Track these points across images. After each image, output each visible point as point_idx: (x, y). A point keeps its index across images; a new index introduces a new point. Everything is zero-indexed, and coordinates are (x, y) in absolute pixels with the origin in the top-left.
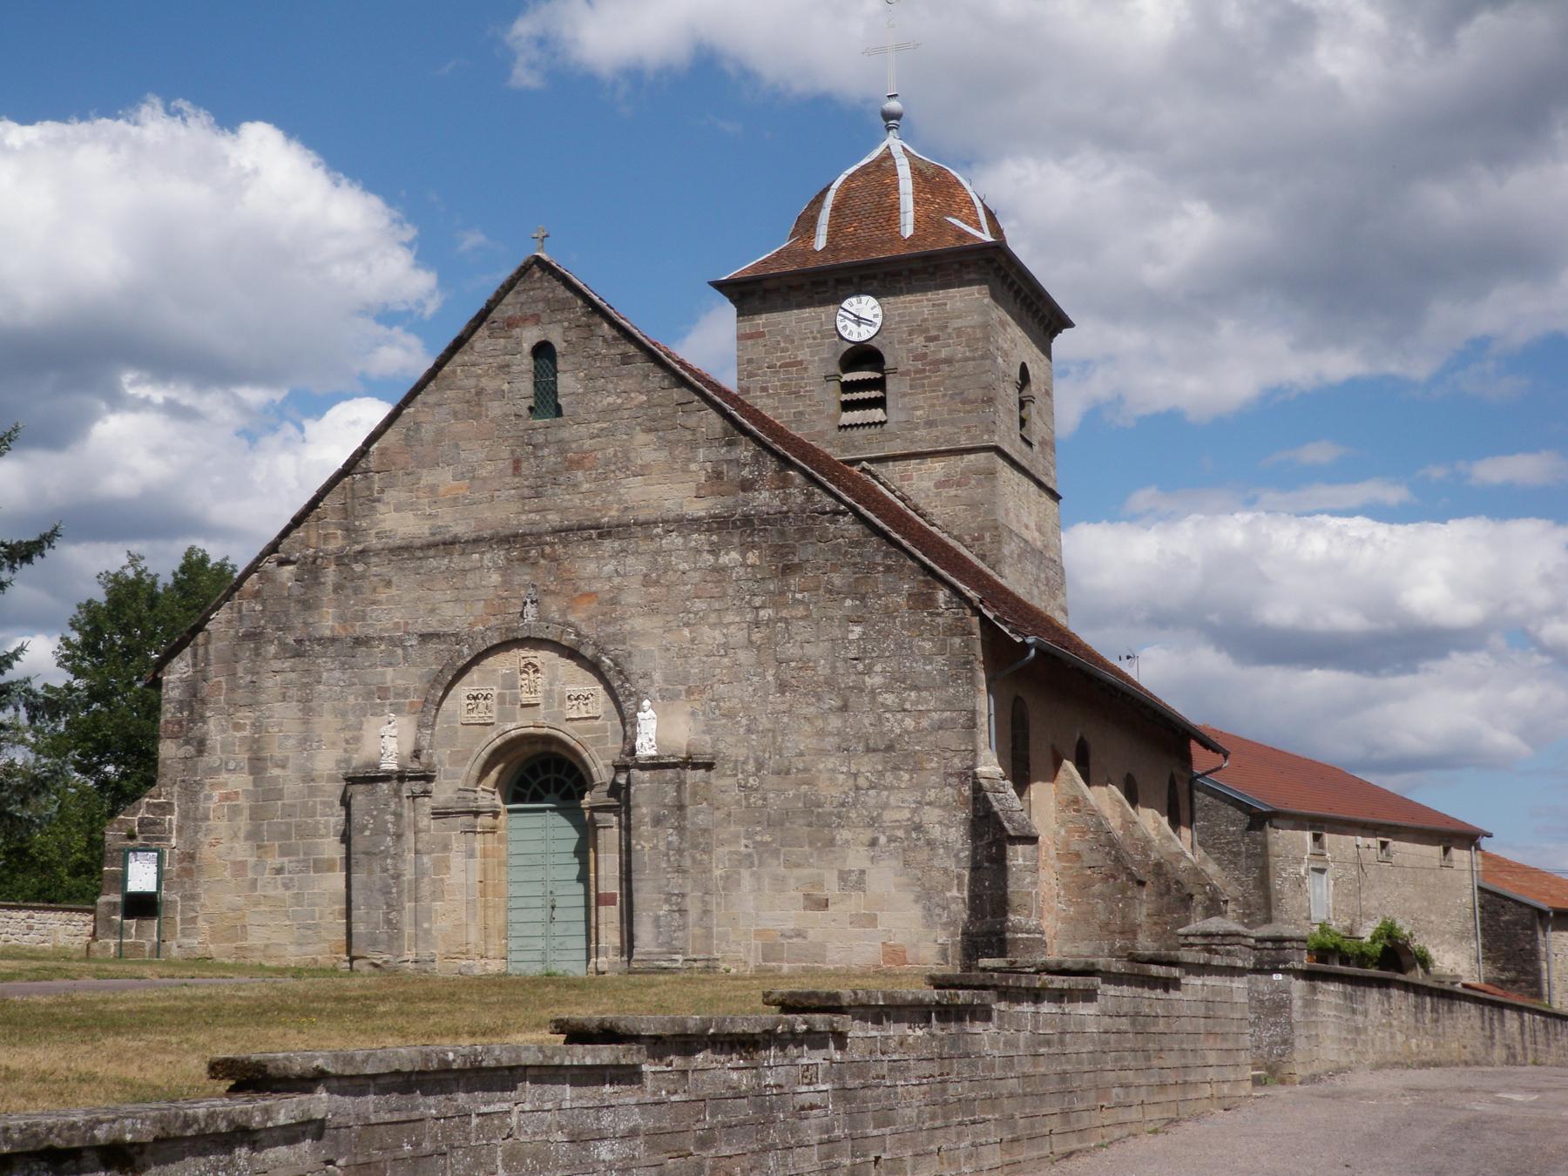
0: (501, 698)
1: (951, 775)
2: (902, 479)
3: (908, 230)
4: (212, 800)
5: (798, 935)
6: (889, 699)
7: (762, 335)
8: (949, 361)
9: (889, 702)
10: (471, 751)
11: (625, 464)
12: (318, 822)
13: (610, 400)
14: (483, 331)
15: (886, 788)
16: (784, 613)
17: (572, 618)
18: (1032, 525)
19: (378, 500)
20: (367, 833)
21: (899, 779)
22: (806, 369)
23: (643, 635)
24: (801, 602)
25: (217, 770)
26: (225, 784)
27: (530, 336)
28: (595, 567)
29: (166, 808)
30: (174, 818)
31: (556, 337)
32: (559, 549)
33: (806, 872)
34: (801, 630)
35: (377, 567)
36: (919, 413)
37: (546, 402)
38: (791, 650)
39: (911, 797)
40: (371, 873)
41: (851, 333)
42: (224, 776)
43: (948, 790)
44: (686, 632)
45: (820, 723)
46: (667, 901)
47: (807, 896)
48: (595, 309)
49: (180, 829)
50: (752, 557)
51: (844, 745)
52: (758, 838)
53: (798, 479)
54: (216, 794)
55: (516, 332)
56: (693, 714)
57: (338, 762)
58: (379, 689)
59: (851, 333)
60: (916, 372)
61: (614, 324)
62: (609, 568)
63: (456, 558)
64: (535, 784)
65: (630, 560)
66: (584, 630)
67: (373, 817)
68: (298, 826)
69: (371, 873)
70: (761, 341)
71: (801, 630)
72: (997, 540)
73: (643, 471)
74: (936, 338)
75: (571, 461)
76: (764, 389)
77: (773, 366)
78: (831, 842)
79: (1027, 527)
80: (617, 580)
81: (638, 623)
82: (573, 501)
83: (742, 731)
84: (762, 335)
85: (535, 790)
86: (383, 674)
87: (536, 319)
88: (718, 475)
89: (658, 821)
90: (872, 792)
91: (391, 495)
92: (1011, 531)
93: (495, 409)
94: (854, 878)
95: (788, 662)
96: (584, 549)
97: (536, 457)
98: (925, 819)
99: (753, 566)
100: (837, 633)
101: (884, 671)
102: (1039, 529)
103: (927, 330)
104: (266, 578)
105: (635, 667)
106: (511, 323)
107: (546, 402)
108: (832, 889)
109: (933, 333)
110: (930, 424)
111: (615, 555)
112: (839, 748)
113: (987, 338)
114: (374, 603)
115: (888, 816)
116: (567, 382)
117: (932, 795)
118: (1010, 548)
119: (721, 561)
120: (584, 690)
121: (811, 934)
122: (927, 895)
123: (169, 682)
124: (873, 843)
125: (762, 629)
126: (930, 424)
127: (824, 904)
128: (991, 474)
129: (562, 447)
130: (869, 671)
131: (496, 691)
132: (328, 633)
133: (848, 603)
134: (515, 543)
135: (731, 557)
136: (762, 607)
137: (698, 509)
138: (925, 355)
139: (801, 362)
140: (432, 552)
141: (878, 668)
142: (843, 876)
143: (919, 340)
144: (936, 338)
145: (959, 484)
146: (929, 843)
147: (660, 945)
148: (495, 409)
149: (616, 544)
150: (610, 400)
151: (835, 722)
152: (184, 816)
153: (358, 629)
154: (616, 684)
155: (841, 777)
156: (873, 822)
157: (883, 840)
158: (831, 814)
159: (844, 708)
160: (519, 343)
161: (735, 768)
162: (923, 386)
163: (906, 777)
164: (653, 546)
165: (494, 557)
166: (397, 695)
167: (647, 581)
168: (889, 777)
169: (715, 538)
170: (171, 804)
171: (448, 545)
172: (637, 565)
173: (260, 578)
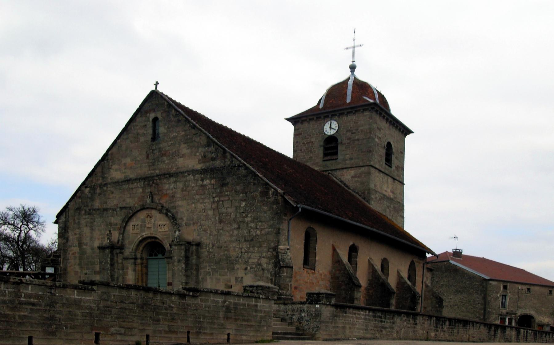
6: (253, 225)
7: (301, 134)
8: (358, 140)
11: (177, 154)
16: (222, 199)
27: (152, 116)
28: (168, 186)
31: (159, 116)
32: (158, 181)
34: (227, 204)
43: (269, 253)
45: (231, 233)
47: (226, 284)
62: (172, 186)
71: (227, 204)
78: (233, 269)
80: (174, 190)
81: (180, 203)
84: (301, 134)
87: (154, 111)
90: (246, 254)
94: (239, 279)
96: (165, 181)
98: (262, 262)
101: (251, 216)
106: (147, 112)
109: (354, 131)
116: (162, 130)
117: (264, 254)
120: (164, 223)
124: (246, 269)
130: (247, 216)
133: (241, 195)
134: (147, 180)
137: (199, 167)
141: (249, 215)
142: (236, 279)
144: (355, 133)
145: (359, 177)
151: (236, 232)
153: (105, 206)
157: (249, 268)
159: (239, 228)
160: (149, 118)
163: (257, 249)
164: (185, 179)
166: (114, 225)
172: (180, 185)
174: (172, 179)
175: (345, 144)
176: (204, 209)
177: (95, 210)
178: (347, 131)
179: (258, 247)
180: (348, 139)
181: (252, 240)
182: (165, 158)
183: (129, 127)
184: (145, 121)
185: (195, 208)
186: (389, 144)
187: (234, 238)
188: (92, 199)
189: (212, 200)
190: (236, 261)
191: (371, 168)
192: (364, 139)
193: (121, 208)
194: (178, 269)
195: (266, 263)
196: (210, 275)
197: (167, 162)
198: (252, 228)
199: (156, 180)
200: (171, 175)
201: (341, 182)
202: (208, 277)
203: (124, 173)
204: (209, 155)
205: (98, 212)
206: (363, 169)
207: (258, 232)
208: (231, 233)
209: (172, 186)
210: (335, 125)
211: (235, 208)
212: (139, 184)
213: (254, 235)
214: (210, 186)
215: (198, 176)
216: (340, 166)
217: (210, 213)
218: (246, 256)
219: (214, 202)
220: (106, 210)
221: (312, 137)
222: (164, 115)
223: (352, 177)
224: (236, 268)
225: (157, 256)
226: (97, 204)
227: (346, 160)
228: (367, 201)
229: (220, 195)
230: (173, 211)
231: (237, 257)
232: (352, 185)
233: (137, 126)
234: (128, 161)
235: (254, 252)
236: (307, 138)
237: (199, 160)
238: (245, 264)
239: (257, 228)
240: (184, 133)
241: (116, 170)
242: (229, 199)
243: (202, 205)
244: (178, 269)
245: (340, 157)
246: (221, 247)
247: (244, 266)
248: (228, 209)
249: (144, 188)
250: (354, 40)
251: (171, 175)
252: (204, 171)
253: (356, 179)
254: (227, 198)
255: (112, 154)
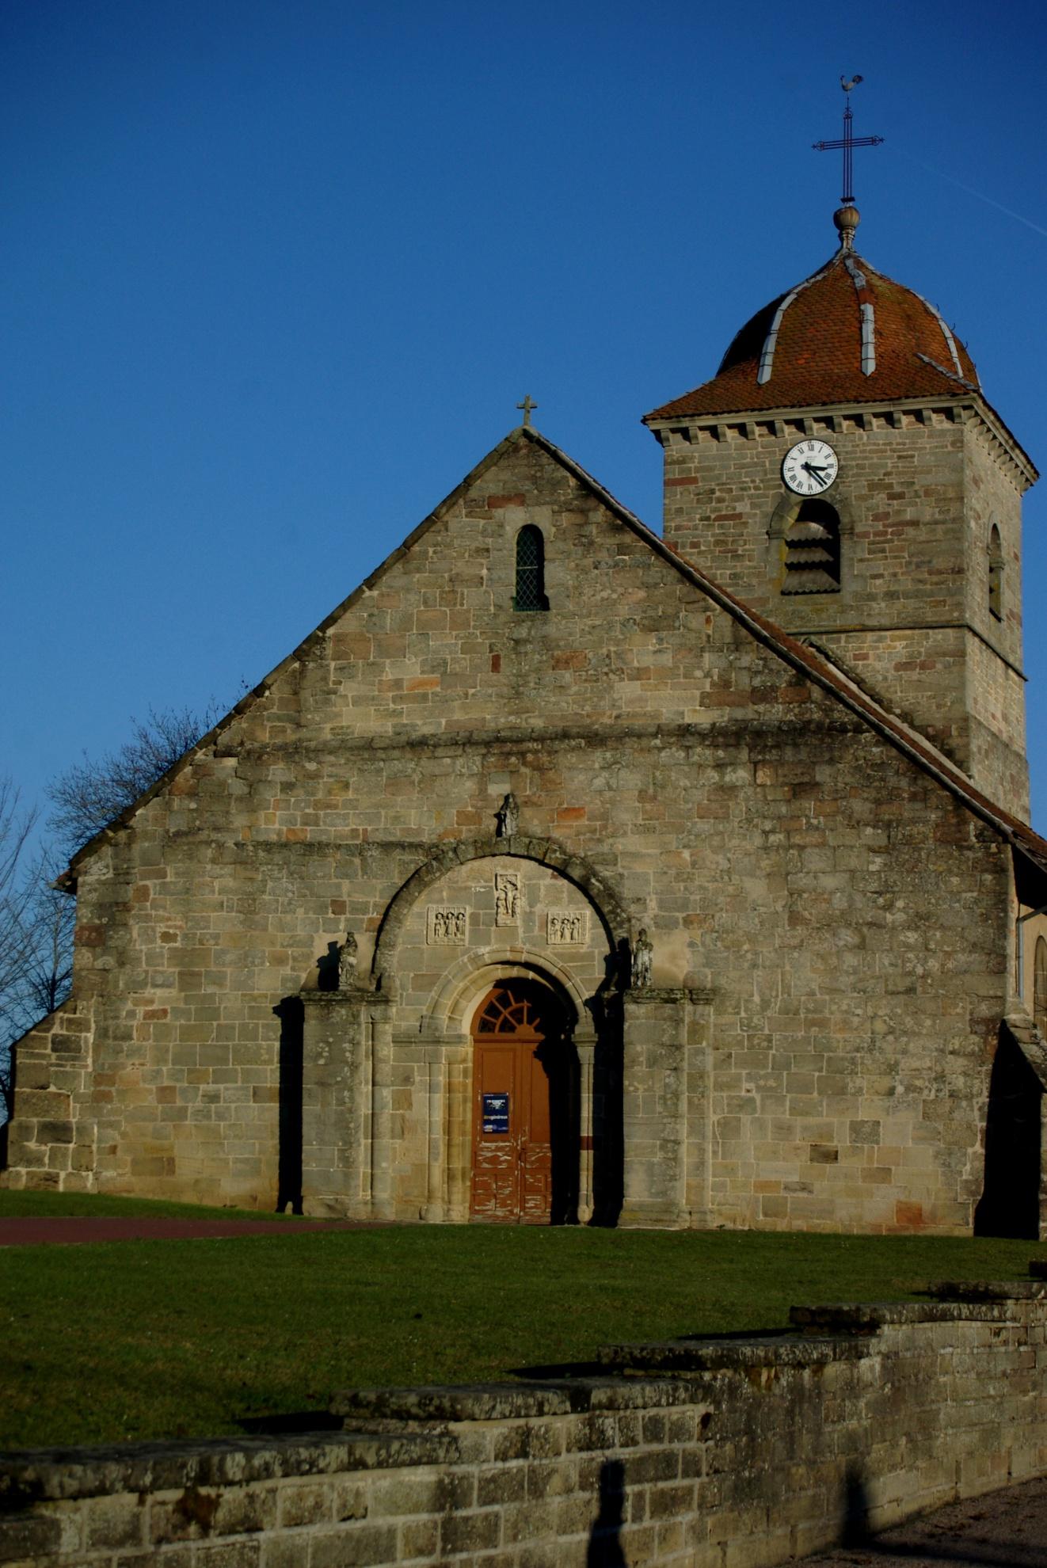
0: (474, 918)
1: (978, 1023)
2: (856, 658)
3: (870, 367)
4: (132, 1012)
5: (803, 1189)
6: (912, 937)
7: (694, 481)
8: (915, 523)
9: (911, 941)
10: (438, 976)
11: (615, 667)
12: (259, 1047)
13: (605, 594)
14: (461, 508)
15: (905, 1033)
16: (797, 839)
17: (556, 834)
18: (999, 715)
19: (335, 693)
20: (322, 1062)
21: (920, 1024)
22: (745, 523)
23: (635, 856)
24: (817, 828)
25: (143, 985)
26: (152, 1002)
27: (515, 518)
28: (583, 777)
29: (81, 1025)
30: (91, 1036)
31: (543, 518)
32: (544, 758)
33: (812, 1120)
34: (815, 860)
35: (333, 766)
36: (879, 582)
37: (532, 595)
38: (803, 881)
39: (932, 1044)
40: (325, 1104)
41: (800, 485)
42: (149, 992)
43: (975, 1039)
44: (686, 854)
45: (834, 961)
46: (662, 1147)
47: (814, 1147)
48: (589, 491)
49: (97, 1048)
50: (763, 776)
51: (860, 986)
52: (762, 1083)
53: (817, 693)
54: (141, 1011)
55: (498, 513)
56: (691, 945)
57: (284, 980)
58: (334, 902)
59: (800, 485)
60: (876, 534)
61: (609, 507)
62: (599, 782)
63: (424, 762)
64: (506, 1013)
65: (623, 773)
66: (570, 849)
67: (328, 1043)
68: (236, 1050)
69: (325, 1104)
70: (692, 487)
71: (815, 860)
72: (964, 730)
73: (639, 674)
74: (901, 496)
75: (558, 661)
76: (695, 545)
77: (708, 518)
78: (842, 1091)
79: (993, 716)
80: (608, 794)
81: (630, 843)
82: (558, 702)
83: (746, 965)
84: (694, 481)
85: (506, 1020)
86: (338, 886)
87: (520, 499)
88: (726, 684)
89: (653, 1061)
90: (890, 1038)
91: (349, 689)
92: (980, 723)
93: (472, 597)
94: (867, 1129)
95: (800, 893)
96: (572, 758)
97: (518, 654)
98: (947, 1067)
99: (763, 786)
100: (854, 863)
101: (904, 910)
102: (1005, 718)
103: (891, 486)
104: (201, 771)
105: (627, 891)
106: (494, 502)
107: (532, 595)
108: (841, 1141)
109: (897, 489)
110: (891, 596)
111: (606, 767)
112: (854, 989)
113: (961, 499)
114: (329, 806)
115: (906, 1063)
116: (556, 574)
117: (956, 1043)
118: (978, 742)
119: (727, 778)
120: (571, 913)
121: (817, 1186)
122: (947, 1157)
123: (84, 884)
124: (891, 1092)
125: (773, 855)
126: (891, 596)
127: (832, 1156)
128: (961, 654)
129: (546, 643)
130: (889, 907)
131: (469, 910)
132: (274, 838)
133: (869, 830)
134: (502, 747)
135: (739, 775)
136: (773, 831)
137: (703, 718)
138: (887, 515)
139: (740, 516)
140: (396, 753)
141: (900, 904)
142: (856, 1128)
143: (880, 498)
144: (901, 496)
145: (923, 666)
146: (952, 1095)
147: (657, 1194)
148: (472, 597)
149: (608, 755)
150: (605, 594)
151: (851, 960)
152: (102, 1034)
153: (310, 834)
154: (606, 909)
155: (856, 1020)
156: (892, 1069)
157: (900, 1089)
158: (843, 1059)
159: (862, 946)
160: (501, 526)
161: (738, 1007)
162: (883, 551)
163: (928, 1023)
164: (650, 759)
165: (471, 762)
166: (354, 911)
167: (642, 796)
168: (909, 1022)
169: (721, 753)
170: (88, 1021)
171: (419, 745)
172: (631, 780)
173: (195, 773)
174: (598, 757)
175: (866, 535)
176: (729, 872)
177: (268, 846)
178: (872, 486)
179: (934, 1016)
180: (876, 518)
181: (910, 990)
182: (567, 676)
183: (416, 548)
184: (484, 533)
185: (694, 864)
186: (995, 527)
187: (845, 981)
188: (250, 801)
189: (758, 841)
190: (853, 1061)
191: (966, 631)
192: (936, 523)
193: (387, 847)
194: (650, 1089)
195: (965, 1074)
196: (754, 1111)
197: (574, 689)
198: (909, 947)
199: (536, 752)
200: (595, 739)
201: (859, 683)
202: (746, 1119)
203: (395, 713)
204: (743, 682)
205: (278, 858)
206: (938, 635)
207: (933, 964)
208: (834, 961)
209: (599, 782)
210: (821, 454)
211: (847, 876)
212: (460, 761)
213: (920, 970)
214: (750, 791)
215: (702, 753)
216: (851, 619)
217: (756, 888)
218: (889, 1045)
219: (766, 849)
220: (314, 848)
221: (739, 499)
222: (566, 519)
223: (899, 667)
224: (851, 1088)
225: (512, 1029)
226: (273, 823)
227: (872, 597)
228: (960, 764)
229: (788, 825)
230: (606, 872)
231: (857, 1050)
232: (901, 695)
233: (449, 546)
234: (411, 669)
235: (919, 1034)
236: (720, 500)
237: (704, 696)
238: (886, 1074)
239: (927, 949)
240: (642, 594)
241: (357, 701)
242: (823, 845)
243: (720, 858)
244: (650, 1089)
245: (850, 585)
246: (797, 1013)
247: (885, 1083)
248: (824, 880)
249: (483, 779)
250: (848, 117)
251: (595, 739)
252: (714, 736)
253: (915, 675)
254: (813, 838)
255: (339, 639)
